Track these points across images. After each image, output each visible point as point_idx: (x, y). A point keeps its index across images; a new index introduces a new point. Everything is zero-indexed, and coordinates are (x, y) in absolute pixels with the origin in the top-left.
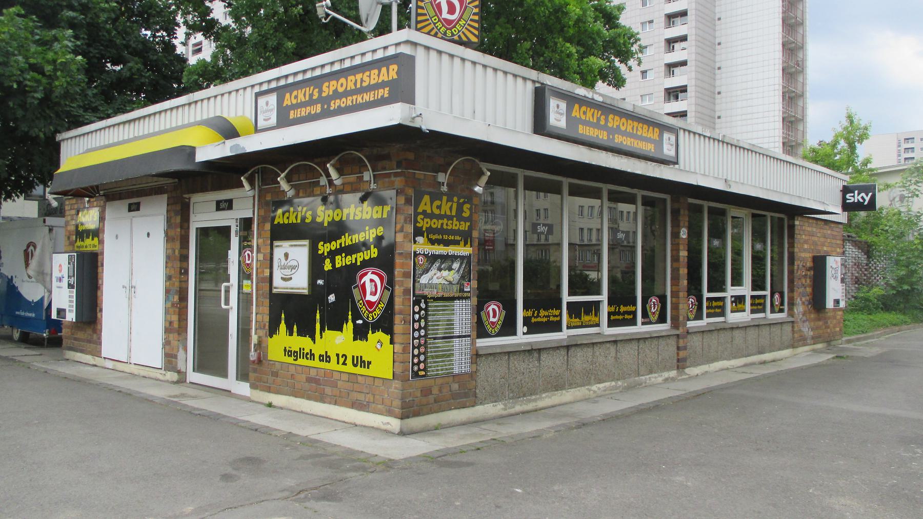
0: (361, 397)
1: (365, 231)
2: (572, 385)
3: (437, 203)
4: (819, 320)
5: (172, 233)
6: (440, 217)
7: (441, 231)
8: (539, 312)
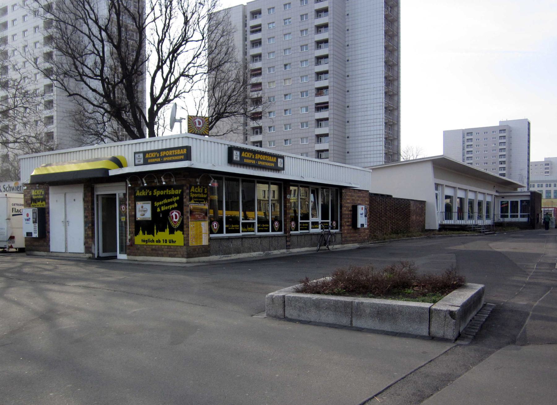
0: (172, 253)
1: (172, 198)
2: (244, 252)
3: (196, 188)
4: (356, 233)
5: (87, 199)
6: (198, 193)
7: (198, 198)
8: (231, 226)
